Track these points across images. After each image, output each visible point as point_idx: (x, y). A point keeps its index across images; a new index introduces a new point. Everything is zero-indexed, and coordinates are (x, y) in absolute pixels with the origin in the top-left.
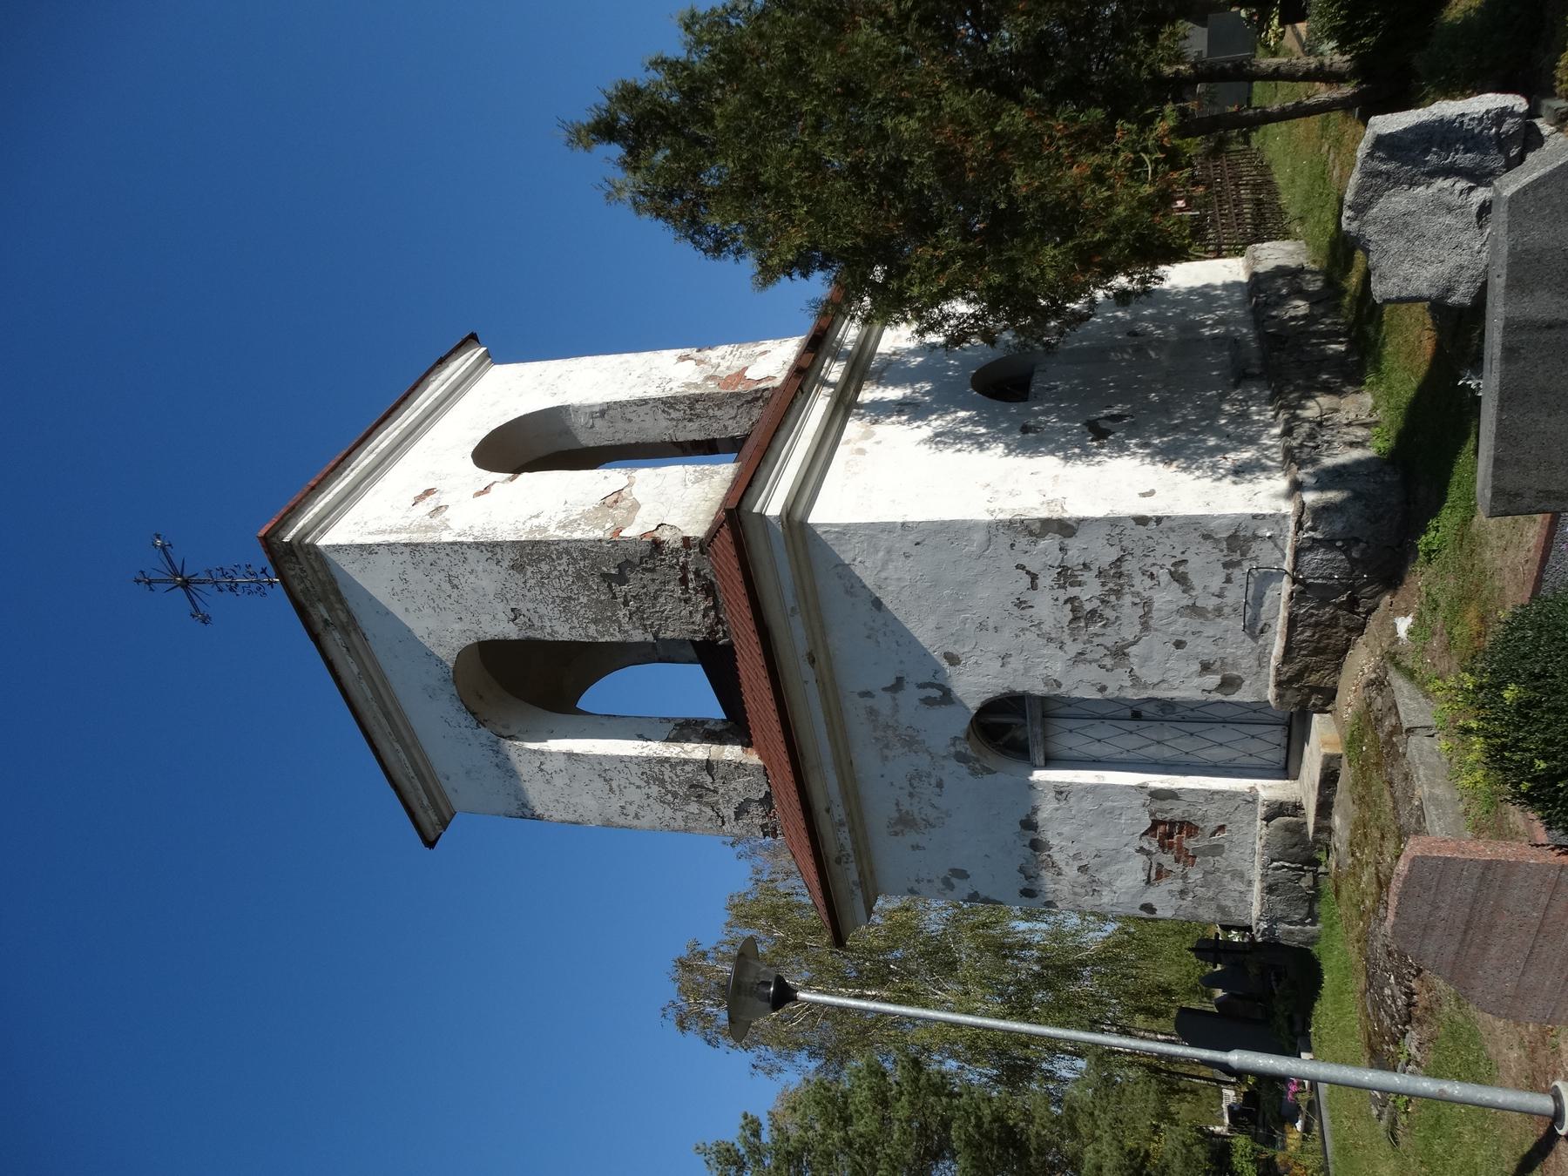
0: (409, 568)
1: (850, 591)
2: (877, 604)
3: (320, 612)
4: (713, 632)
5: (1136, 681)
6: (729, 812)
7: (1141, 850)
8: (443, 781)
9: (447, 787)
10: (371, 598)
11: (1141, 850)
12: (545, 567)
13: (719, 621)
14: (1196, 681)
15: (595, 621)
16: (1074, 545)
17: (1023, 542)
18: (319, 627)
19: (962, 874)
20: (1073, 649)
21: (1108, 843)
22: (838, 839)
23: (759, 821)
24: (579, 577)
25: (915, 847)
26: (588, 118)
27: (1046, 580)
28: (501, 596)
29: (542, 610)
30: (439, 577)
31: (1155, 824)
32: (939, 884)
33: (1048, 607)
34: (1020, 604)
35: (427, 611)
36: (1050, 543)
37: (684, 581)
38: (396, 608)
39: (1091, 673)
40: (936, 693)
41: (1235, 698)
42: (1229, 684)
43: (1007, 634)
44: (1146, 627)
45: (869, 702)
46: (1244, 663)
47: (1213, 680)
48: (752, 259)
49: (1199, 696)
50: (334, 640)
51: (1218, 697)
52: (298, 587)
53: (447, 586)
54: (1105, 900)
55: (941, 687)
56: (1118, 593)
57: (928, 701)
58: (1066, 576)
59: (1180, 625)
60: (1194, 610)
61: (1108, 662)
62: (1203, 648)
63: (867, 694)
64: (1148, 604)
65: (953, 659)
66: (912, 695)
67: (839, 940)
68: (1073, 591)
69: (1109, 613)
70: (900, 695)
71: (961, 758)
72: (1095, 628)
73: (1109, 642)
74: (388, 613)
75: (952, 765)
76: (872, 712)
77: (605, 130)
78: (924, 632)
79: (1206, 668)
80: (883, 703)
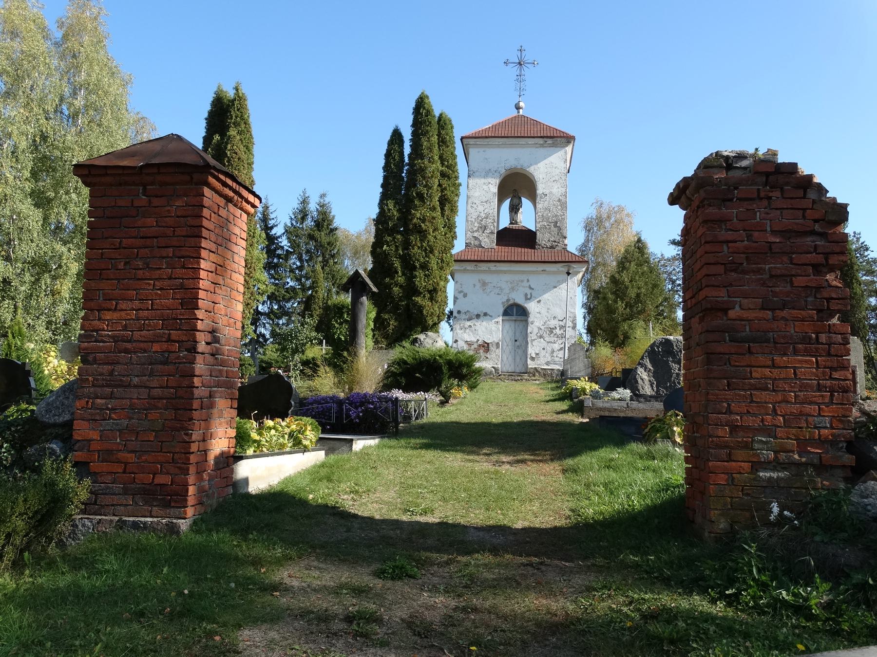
0: (560, 171)
1: (558, 281)
2: (555, 287)
3: (550, 141)
4: (539, 245)
5: (533, 340)
6: (476, 234)
7: (478, 340)
8: (483, 149)
9: (481, 150)
10: (550, 156)
11: (478, 340)
12: (559, 207)
13: (543, 248)
14: (533, 352)
15: (542, 215)
16: (570, 329)
17: (571, 319)
18: (545, 139)
19: (465, 295)
20: (542, 327)
21: (480, 332)
22: (484, 266)
23: (472, 243)
24: (556, 216)
25: (474, 285)
26: (642, 238)
27: (561, 323)
28: (551, 193)
29: (546, 202)
30: (557, 178)
31: (488, 344)
32: (460, 290)
33: (553, 323)
34: (555, 318)
35: (546, 170)
36: (571, 324)
37: (555, 242)
38: (546, 161)
39: (536, 331)
40: (529, 297)
41: (529, 360)
42: (533, 359)
43: (547, 314)
44: (548, 342)
45: (526, 281)
46: (538, 362)
47: (534, 356)
48: (312, 209)
49: (529, 353)
50: (541, 141)
51: (529, 356)
52: (559, 139)
53: (554, 179)
54: (459, 331)
55: (531, 298)
56: (558, 337)
57: (526, 295)
58: (561, 327)
59: (549, 349)
60: (553, 351)
61: (539, 335)
62: (543, 353)
63: (528, 281)
64: (555, 343)
65: (539, 302)
66: (529, 291)
67: (455, 261)
68: (558, 328)
69: (552, 335)
70: (528, 289)
71: (508, 300)
72: (548, 332)
73: (544, 335)
74: (545, 159)
75: (505, 298)
76: (522, 281)
77: (639, 240)
78: (546, 296)
79: (537, 354)
80: (526, 284)
